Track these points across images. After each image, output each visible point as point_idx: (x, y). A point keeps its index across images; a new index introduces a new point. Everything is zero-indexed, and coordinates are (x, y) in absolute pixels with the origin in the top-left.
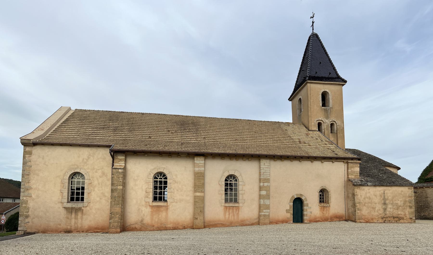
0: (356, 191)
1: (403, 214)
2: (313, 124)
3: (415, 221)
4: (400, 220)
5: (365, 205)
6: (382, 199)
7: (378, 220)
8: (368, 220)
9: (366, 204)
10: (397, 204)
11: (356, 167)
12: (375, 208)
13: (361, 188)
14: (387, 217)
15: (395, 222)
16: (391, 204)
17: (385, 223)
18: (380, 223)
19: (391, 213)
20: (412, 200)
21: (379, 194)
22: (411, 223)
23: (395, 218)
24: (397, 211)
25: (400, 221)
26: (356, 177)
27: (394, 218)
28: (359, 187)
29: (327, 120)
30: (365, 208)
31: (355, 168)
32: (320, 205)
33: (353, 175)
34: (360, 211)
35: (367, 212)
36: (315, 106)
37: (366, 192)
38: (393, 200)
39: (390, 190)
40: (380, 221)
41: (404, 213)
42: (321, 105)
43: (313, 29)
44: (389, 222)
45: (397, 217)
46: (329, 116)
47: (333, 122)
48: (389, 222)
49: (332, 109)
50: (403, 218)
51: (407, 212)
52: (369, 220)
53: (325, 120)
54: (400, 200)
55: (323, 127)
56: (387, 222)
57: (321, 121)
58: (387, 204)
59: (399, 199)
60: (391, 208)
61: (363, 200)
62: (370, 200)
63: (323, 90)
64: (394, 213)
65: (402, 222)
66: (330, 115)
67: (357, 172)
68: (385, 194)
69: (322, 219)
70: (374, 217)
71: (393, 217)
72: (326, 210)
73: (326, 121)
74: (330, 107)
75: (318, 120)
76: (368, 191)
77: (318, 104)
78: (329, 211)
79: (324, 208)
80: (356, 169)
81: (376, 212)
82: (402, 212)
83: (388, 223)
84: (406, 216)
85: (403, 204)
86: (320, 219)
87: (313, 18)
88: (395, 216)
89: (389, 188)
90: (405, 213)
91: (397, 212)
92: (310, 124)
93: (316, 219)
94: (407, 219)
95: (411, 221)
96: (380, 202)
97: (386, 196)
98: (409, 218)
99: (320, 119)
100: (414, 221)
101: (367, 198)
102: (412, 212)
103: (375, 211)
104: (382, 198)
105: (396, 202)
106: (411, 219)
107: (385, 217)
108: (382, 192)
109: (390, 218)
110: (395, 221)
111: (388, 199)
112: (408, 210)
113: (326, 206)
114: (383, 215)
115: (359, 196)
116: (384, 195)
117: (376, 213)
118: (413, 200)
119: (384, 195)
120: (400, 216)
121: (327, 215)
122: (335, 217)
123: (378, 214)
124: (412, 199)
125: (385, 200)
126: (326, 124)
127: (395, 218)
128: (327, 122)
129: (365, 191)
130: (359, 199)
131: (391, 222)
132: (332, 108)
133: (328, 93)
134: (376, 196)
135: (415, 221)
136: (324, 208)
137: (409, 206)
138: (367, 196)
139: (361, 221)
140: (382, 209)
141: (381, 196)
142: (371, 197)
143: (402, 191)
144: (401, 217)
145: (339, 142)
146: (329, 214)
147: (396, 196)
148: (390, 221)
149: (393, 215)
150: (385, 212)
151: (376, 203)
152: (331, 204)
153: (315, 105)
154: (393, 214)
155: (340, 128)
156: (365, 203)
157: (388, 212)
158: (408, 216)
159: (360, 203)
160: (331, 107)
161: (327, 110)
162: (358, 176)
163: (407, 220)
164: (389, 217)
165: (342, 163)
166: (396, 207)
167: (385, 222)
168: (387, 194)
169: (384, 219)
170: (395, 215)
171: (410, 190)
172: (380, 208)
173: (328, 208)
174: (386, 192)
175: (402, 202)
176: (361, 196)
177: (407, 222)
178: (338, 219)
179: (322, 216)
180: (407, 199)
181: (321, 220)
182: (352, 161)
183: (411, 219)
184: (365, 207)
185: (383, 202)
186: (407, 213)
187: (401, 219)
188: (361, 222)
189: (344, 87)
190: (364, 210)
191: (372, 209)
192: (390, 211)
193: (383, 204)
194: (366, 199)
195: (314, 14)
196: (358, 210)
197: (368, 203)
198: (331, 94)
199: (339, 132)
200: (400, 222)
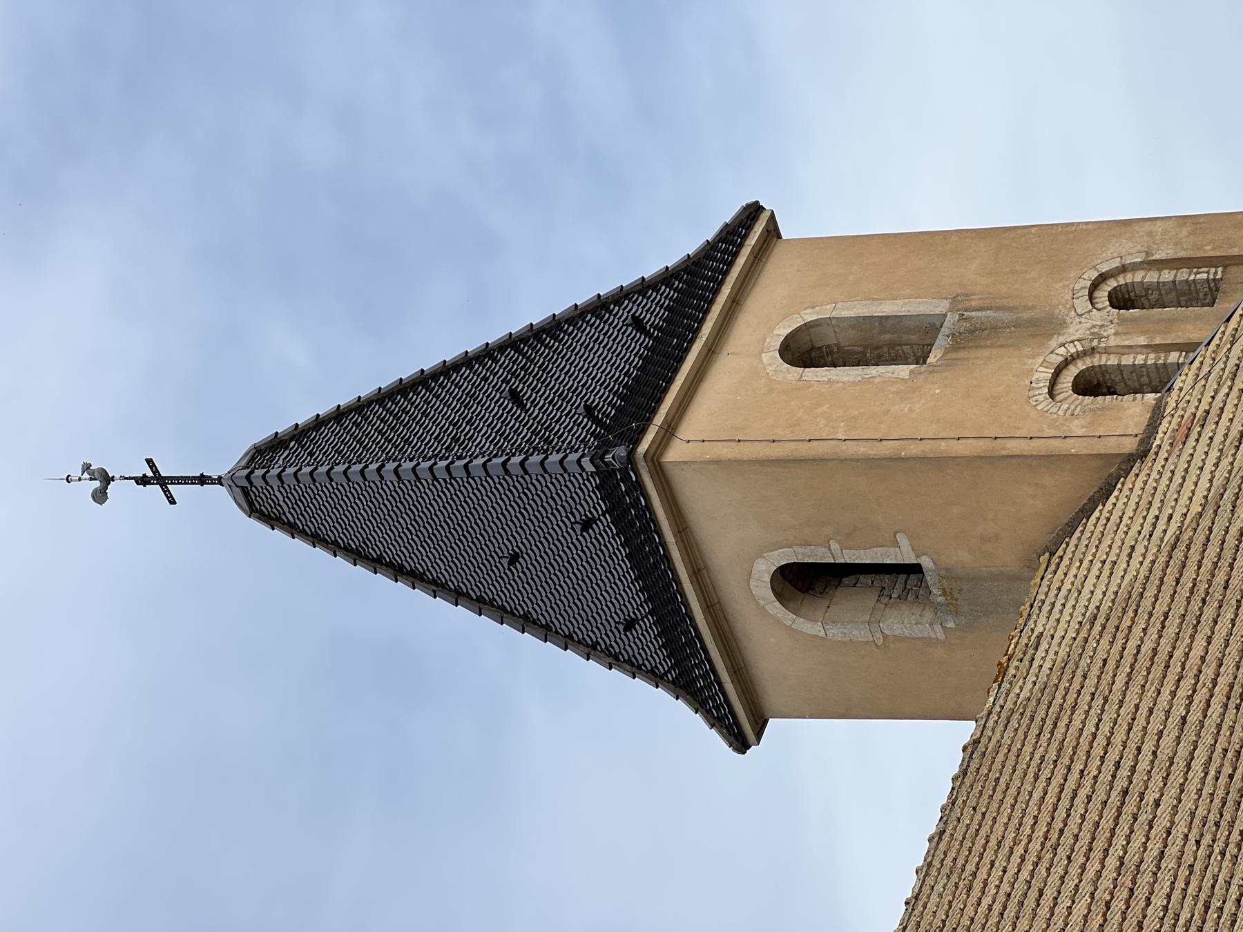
2: (1077, 428)
43: (202, 480)
46: (1026, 315)
53: (1062, 339)
55: (1127, 360)
57: (1061, 379)
63: (765, 357)
73: (1078, 336)
87: (107, 479)
92: (1075, 447)
99: (1047, 374)
133: (808, 326)
189: (788, 231)
195: (87, 467)
199: (1214, 249)
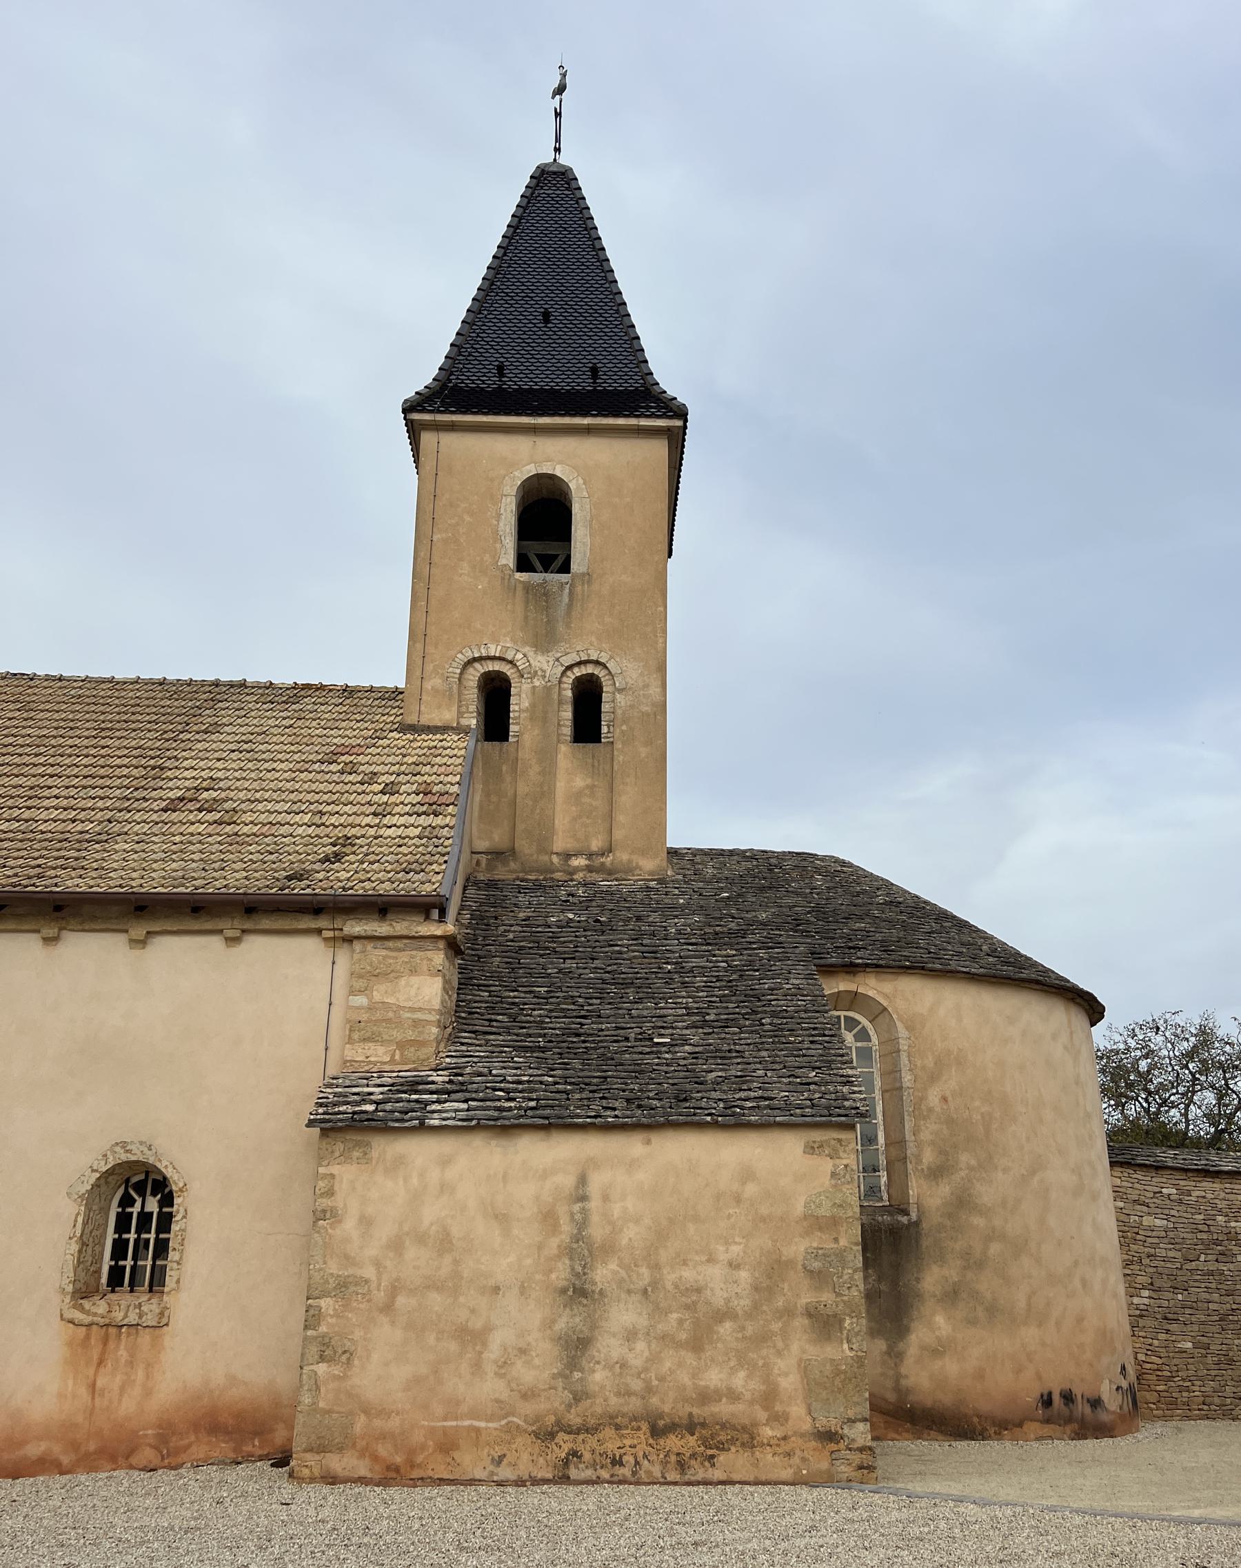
0: (332, 1176)
1: (748, 1396)
3: (865, 1458)
4: (722, 1447)
5: (388, 1308)
6: (555, 1252)
7: (497, 1453)
8: (398, 1459)
9: (401, 1300)
10: (699, 1291)
11: (414, 971)
12: (488, 1329)
13: (375, 1154)
14: (592, 1422)
15: (672, 1476)
16: (636, 1298)
17: (565, 1480)
18: (519, 1483)
19: (636, 1385)
20: (841, 1255)
21: (537, 1198)
22: (827, 1480)
23: (672, 1428)
24: (689, 1358)
25: (722, 1458)
26: (410, 1053)
27: (657, 1432)
28: (358, 1144)
29: (540, 658)
30: (386, 1334)
31: (403, 982)
32: (78, 1316)
33: (383, 1042)
34: (336, 1370)
35: (402, 1373)
36: (465, 567)
37: (415, 1181)
38: (664, 1256)
39: (632, 1165)
40: (523, 1470)
41: (756, 1385)
42: (508, 558)
44: (605, 1474)
45: (691, 1426)
46: (561, 628)
47: (589, 669)
48: (605, 1474)
49: (589, 582)
50: (744, 1429)
51: (786, 1375)
52: (412, 1452)
53: (531, 654)
54: (723, 1257)
56: (589, 1474)
58: (601, 1292)
59: (721, 1248)
60: (630, 1336)
61: (378, 1264)
62: (447, 1260)
64: (662, 1379)
65: (736, 1477)
66: (568, 626)
67: (419, 1015)
68: (583, 1198)
69: (74, 1446)
70: (467, 1423)
71: (645, 1427)
72: (123, 1354)
74: (576, 575)
75: (475, 660)
76: (434, 1175)
77: (487, 557)
78: (149, 1366)
79: (105, 1341)
80: (413, 992)
81: (490, 1369)
82: (742, 1374)
83: (597, 1481)
84: (778, 1408)
85: (756, 1289)
86: (57, 1449)
88: (667, 1408)
89: (632, 1146)
90: (768, 1380)
91: (694, 1376)
93: (22, 1443)
94: (785, 1438)
95: (824, 1465)
96: (538, 1277)
97: (595, 1218)
98: (807, 1426)
99: (494, 650)
100: (856, 1458)
101: (421, 1239)
102: (838, 1373)
103: (477, 1367)
104: (554, 1242)
105: (688, 1274)
106: (833, 1446)
107: (574, 1419)
108: (567, 1181)
109: (618, 1427)
110: (665, 1463)
111: (608, 1249)
112: (795, 1347)
113: (133, 1318)
114: (553, 1403)
115: (349, 1225)
116: (577, 1207)
117: (491, 1388)
118: (851, 1257)
119: (584, 1211)
120: (724, 1409)
121: (128, 1406)
122: (196, 1427)
123: (505, 1395)
124: (843, 1242)
125: (583, 1258)
126: (537, 683)
127: (672, 1428)
128: (545, 667)
129: (405, 1180)
130: (347, 1257)
131: (625, 1472)
132: (587, 577)
134: (502, 1219)
135: (865, 1458)
136: (111, 1345)
137: (812, 1313)
138: (426, 1223)
139: (337, 1463)
140: (547, 1345)
141: (548, 1218)
142: (456, 1232)
143: (747, 1175)
144: (723, 1426)
145: (624, 798)
146: (148, 1393)
147: (696, 1219)
148: (617, 1462)
149: (654, 1400)
150: (577, 1375)
151: (496, 1289)
152: (183, 1296)
153: (465, 565)
154: (649, 1390)
155: (632, 707)
156: (394, 1288)
157: (599, 1376)
158: (797, 1410)
159: (352, 1289)
160: (583, 574)
161: (545, 594)
162: (421, 1044)
163: (786, 1447)
164: (614, 1422)
165: (311, 944)
166: (687, 1325)
167: (573, 1473)
168: (606, 1198)
169: (565, 1443)
170: (667, 1404)
171: (827, 1165)
172: (530, 1339)
173: (145, 1338)
174: (596, 1182)
175: (744, 1275)
176: (366, 1222)
177: (787, 1474)
178: (224, 1448)
179: (80, 1419)
180: (798, 1248)
181: (66, 1460)
182: (382, 928)
183: (828, 1436)
184: (393, 1323)
185: (561, 1274)
186: (789, 1382)
187: (733, 1441)
188: (331, 1479)
190: (375, 1356)
191: (453, 1346)
192: (624, 1365)
193: (564, 1291)
194: (411, 1252)
196: (322, 1359)
197: (428, 1287)
198: (585, 494)
200: (718, 1474)
